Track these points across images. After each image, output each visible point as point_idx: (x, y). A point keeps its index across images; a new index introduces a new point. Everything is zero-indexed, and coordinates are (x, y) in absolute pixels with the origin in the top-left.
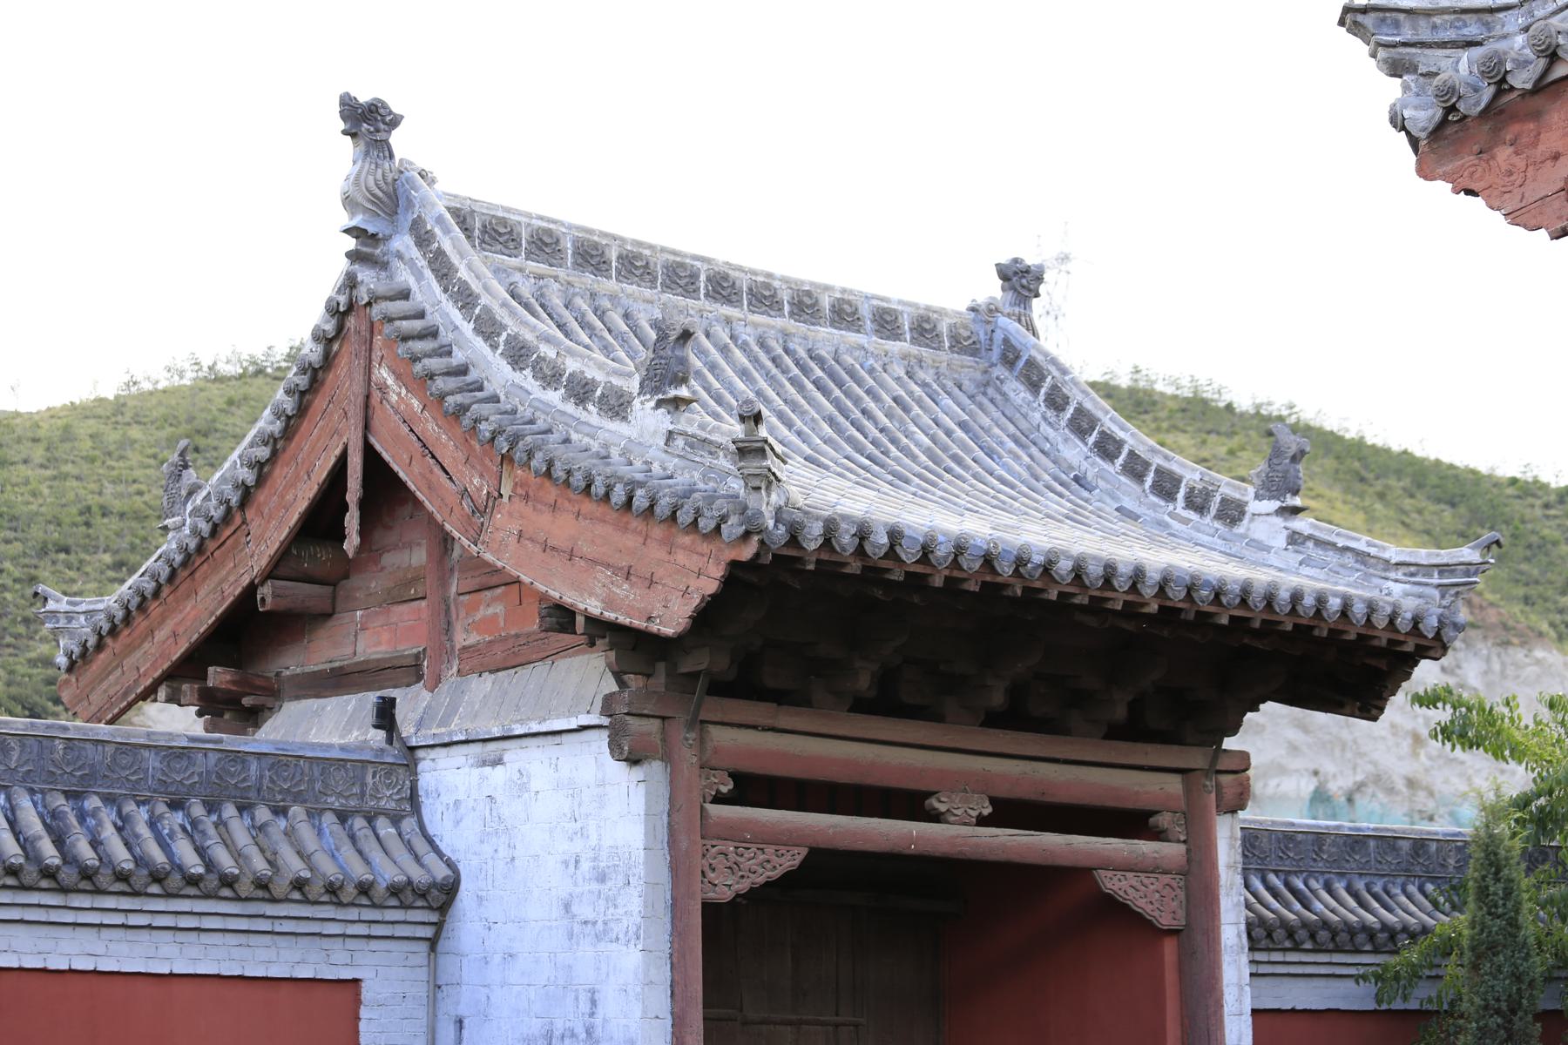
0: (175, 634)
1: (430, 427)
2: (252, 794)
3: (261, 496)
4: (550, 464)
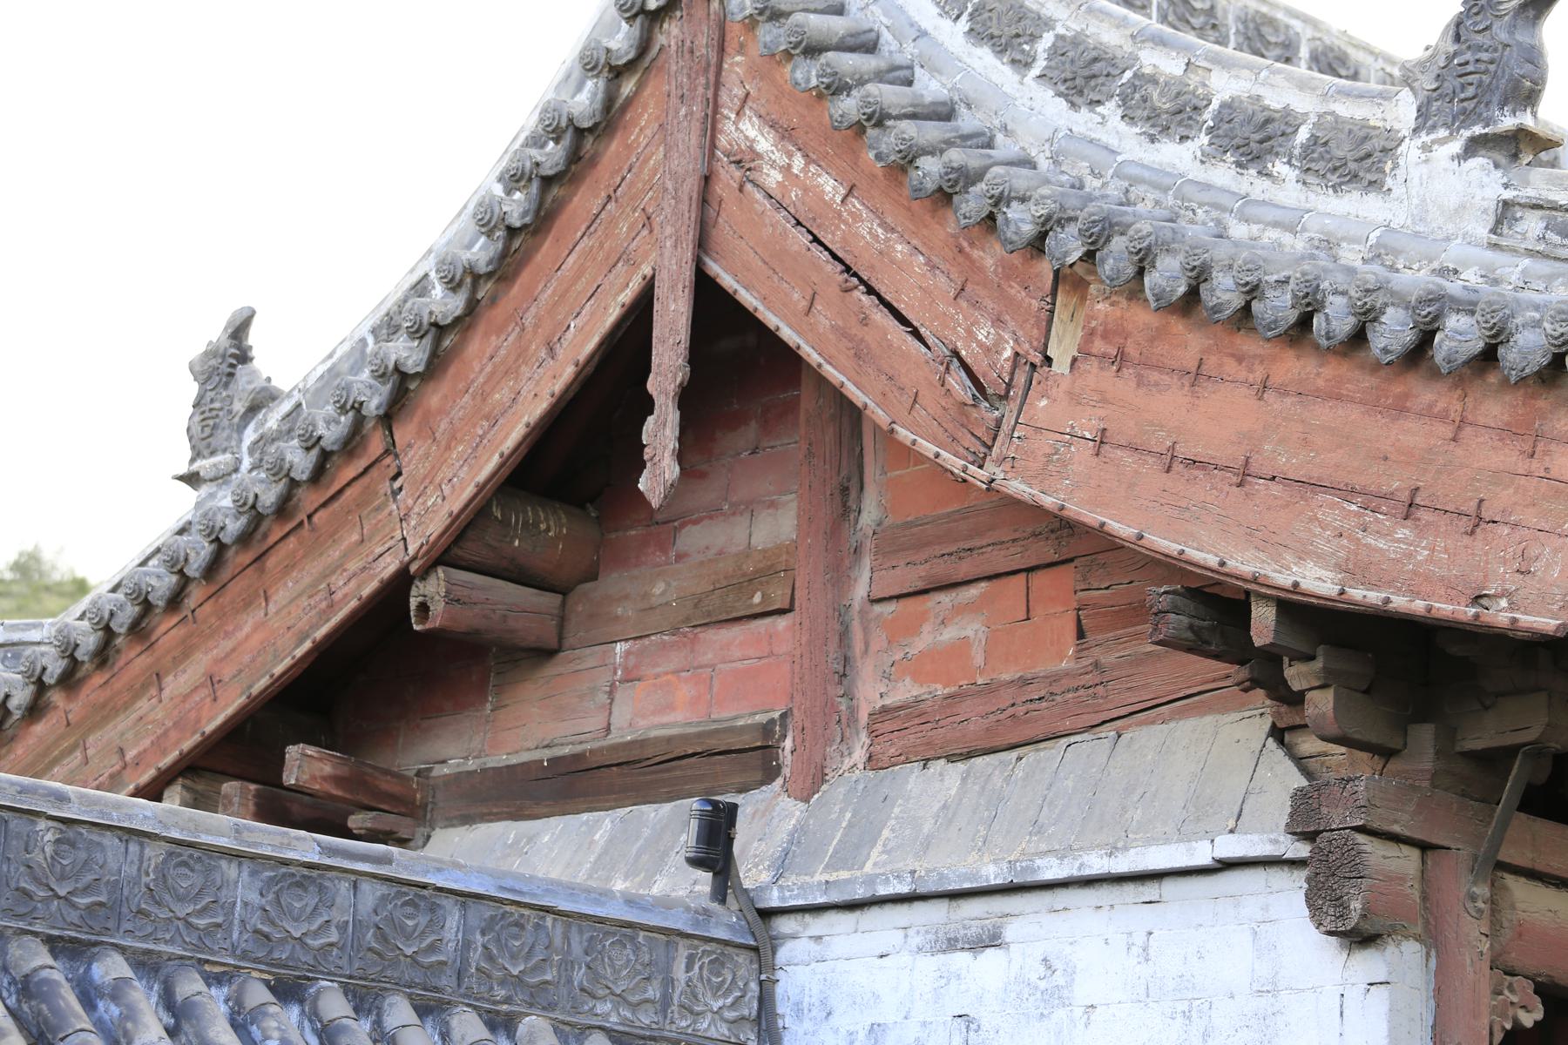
0: (212, 680)
1: (867, 231)
2: (447, 981)
3: (434, 397)
4: (1199, 277)
